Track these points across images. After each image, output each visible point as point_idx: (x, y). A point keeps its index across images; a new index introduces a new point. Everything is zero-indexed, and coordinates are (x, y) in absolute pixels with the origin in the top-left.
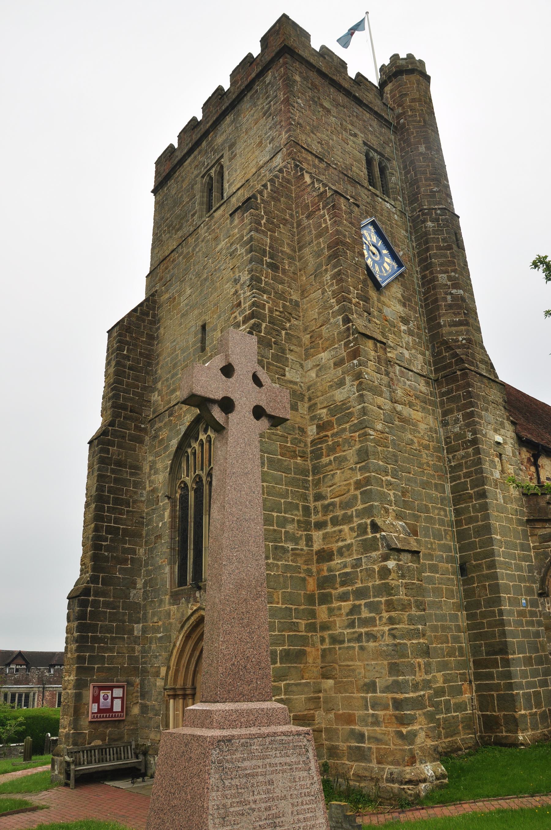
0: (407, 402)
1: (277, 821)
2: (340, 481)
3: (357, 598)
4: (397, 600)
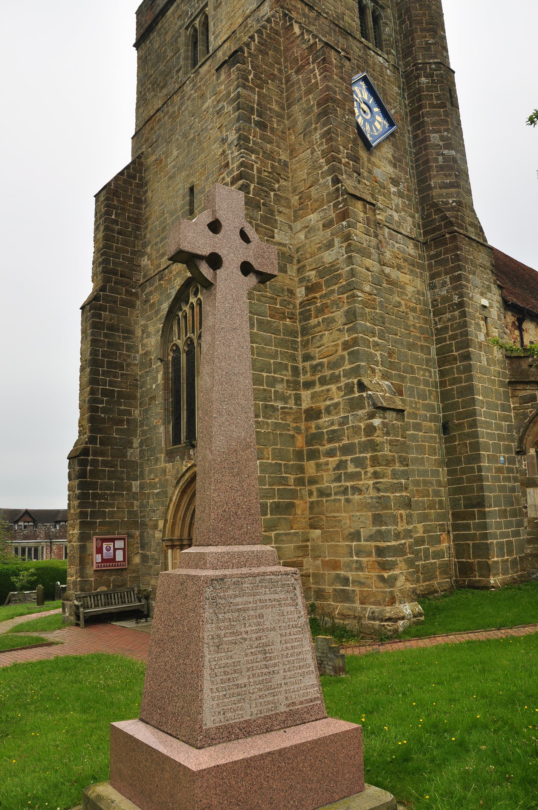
0: (395, 265)
1: (267, 648)
2: (328, 342)
3: (344, 453)
4: (381, 456)
